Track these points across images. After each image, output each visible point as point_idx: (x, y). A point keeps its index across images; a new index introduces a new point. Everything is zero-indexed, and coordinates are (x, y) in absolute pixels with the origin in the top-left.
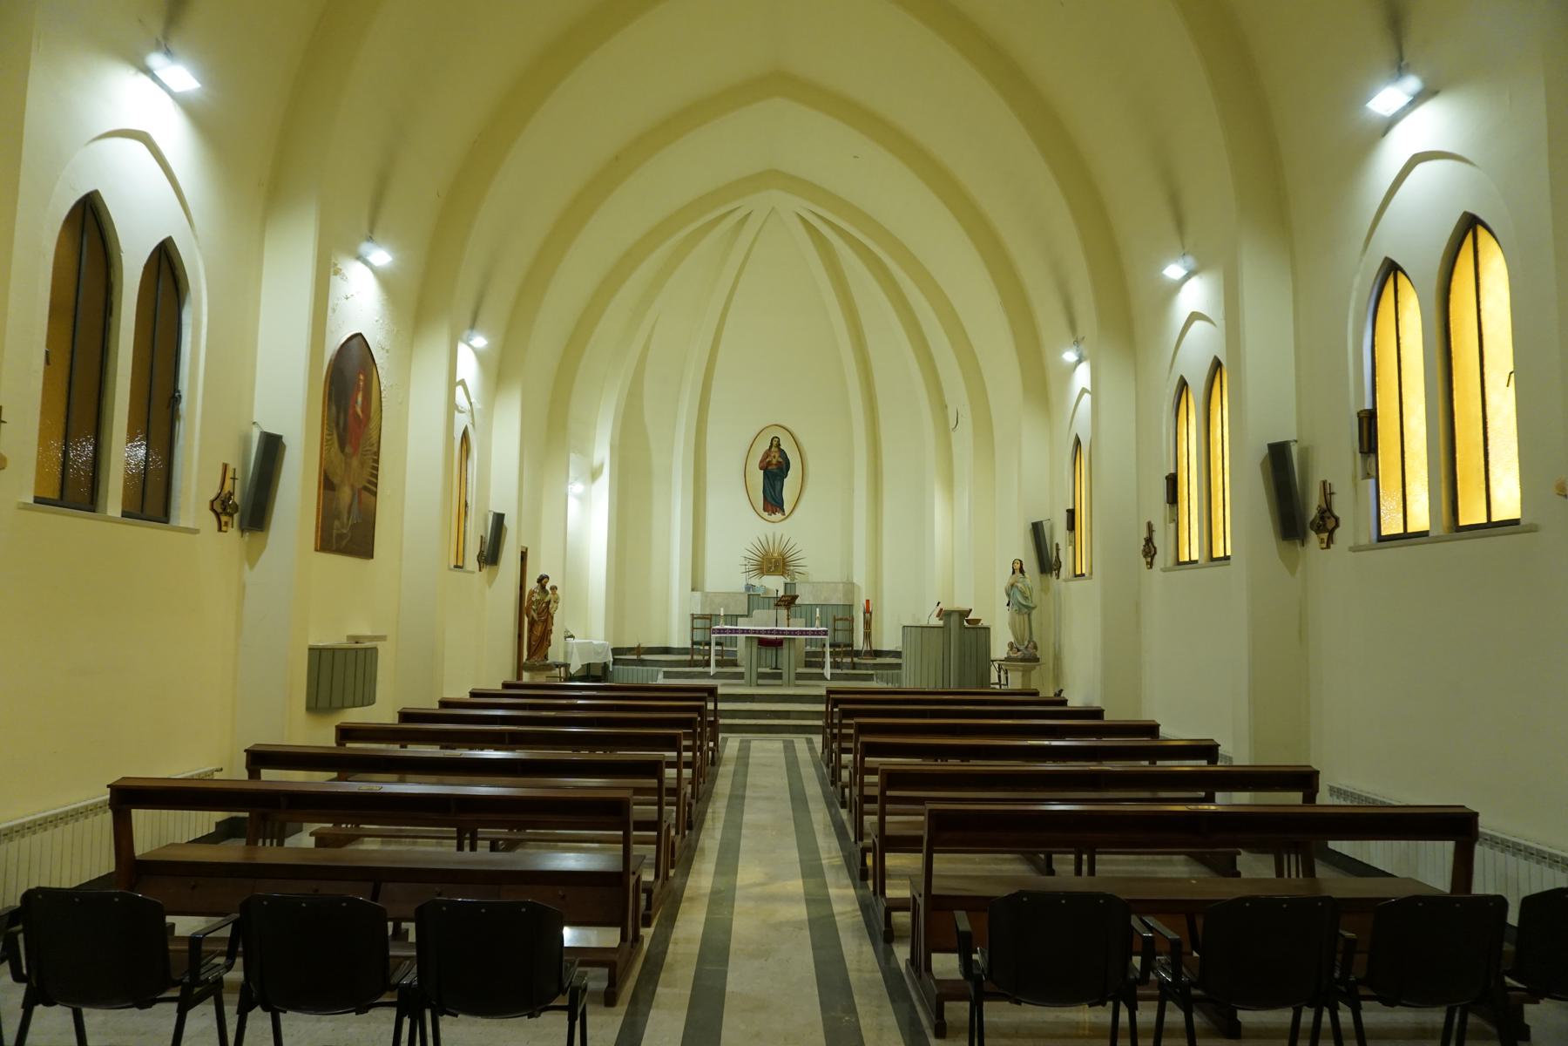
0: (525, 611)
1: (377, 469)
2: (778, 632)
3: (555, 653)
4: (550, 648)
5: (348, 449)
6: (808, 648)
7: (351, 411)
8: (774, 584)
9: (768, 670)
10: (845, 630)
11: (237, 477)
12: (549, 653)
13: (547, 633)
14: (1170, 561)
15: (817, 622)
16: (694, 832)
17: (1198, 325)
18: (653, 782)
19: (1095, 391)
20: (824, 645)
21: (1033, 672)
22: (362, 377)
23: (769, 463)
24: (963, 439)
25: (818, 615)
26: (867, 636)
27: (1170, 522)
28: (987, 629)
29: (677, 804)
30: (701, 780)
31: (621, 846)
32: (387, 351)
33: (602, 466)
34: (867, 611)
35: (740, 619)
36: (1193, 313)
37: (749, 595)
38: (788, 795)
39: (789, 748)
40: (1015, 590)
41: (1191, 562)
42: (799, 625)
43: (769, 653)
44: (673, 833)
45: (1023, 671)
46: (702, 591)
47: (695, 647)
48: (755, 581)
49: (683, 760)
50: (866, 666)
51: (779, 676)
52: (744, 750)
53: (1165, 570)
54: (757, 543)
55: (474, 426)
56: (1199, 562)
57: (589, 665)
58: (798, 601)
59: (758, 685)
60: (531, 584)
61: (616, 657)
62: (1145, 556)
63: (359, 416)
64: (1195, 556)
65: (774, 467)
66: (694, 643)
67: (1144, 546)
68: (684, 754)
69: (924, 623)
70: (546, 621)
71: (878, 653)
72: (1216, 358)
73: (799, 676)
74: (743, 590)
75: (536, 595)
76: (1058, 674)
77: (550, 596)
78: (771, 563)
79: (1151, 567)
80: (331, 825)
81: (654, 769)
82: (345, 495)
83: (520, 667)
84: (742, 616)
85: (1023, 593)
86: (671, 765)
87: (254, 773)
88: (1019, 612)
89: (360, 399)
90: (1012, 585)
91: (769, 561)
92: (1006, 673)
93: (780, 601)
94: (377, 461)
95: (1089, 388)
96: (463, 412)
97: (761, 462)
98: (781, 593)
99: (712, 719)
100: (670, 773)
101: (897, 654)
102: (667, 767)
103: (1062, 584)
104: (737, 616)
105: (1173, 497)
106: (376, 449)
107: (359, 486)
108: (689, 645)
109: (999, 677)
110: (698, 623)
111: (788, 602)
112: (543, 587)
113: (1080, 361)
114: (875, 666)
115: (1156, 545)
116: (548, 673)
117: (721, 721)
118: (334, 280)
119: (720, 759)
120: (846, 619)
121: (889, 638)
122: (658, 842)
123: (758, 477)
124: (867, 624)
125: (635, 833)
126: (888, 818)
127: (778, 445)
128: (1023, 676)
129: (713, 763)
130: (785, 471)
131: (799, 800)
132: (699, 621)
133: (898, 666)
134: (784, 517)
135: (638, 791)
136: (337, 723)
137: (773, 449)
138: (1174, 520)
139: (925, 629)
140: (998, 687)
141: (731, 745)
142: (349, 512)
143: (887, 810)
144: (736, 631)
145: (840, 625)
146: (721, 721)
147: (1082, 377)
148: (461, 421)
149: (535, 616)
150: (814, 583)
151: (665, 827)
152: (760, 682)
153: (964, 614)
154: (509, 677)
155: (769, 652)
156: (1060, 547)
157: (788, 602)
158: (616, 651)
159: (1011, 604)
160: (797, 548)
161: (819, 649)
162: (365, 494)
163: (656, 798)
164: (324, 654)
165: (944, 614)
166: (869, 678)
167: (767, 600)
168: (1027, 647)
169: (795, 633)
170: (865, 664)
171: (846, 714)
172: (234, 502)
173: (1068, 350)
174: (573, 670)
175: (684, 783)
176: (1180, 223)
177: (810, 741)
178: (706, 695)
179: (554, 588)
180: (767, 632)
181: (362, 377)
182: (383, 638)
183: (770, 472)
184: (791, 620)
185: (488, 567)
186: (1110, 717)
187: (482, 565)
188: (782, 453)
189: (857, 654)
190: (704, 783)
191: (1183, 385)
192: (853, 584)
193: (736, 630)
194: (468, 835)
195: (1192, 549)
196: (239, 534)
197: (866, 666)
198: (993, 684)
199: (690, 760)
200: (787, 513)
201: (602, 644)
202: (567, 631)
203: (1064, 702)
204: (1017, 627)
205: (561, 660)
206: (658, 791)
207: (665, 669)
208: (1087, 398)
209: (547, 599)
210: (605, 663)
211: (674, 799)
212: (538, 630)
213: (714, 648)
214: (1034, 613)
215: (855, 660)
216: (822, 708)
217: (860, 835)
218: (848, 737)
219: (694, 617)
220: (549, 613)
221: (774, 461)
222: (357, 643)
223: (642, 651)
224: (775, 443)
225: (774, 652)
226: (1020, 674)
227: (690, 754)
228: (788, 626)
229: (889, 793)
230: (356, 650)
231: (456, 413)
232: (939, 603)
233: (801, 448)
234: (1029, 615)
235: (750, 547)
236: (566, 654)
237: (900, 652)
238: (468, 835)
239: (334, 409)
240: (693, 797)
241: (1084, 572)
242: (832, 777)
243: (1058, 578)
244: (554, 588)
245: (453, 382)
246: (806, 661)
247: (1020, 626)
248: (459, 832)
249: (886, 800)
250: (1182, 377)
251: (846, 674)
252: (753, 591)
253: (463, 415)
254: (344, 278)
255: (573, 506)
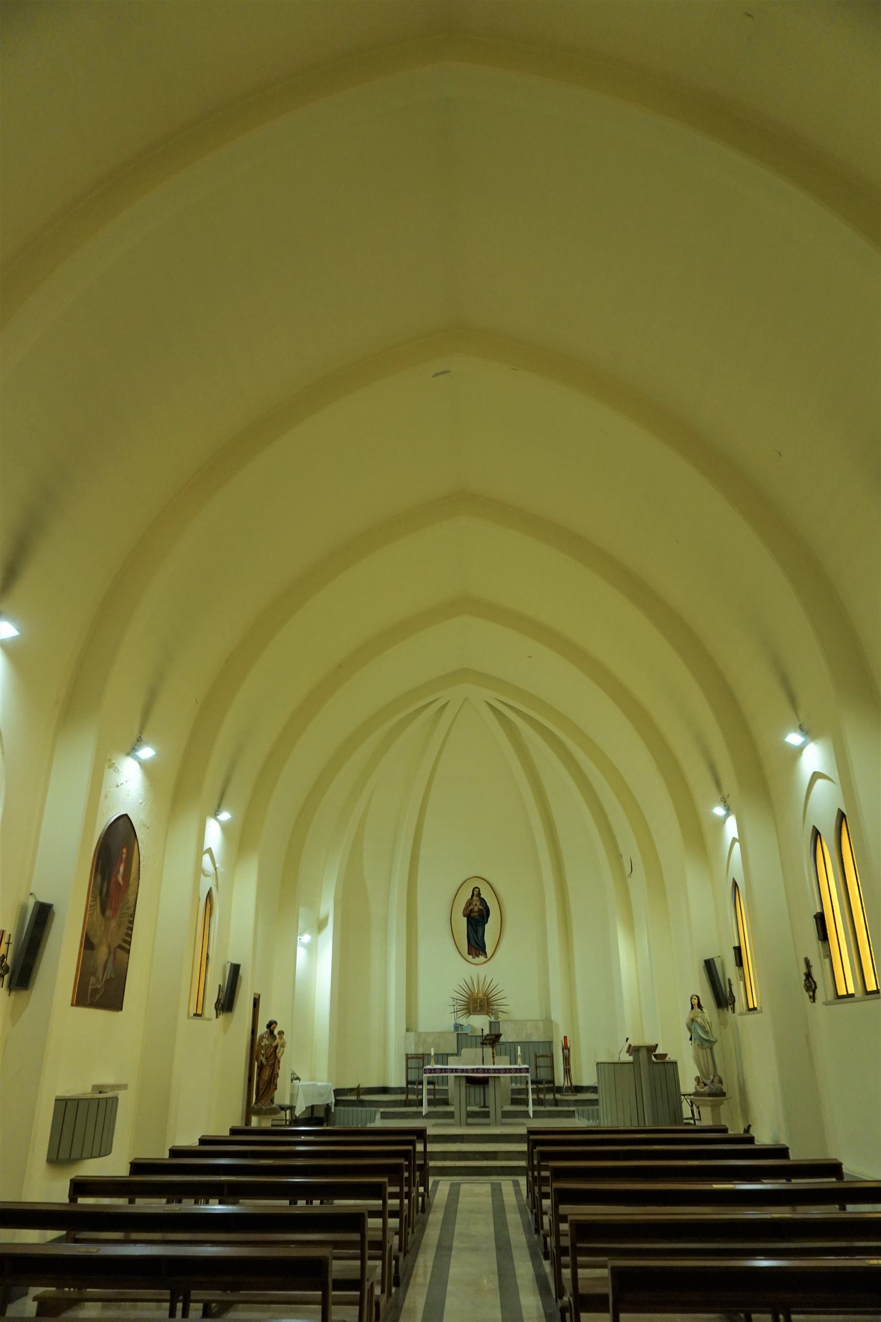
0: (255, 1056)
1: (131, 929)
2: (484, 1071)
3: (282, 1095)
4: (276, 1092)
5: (109, 913)
6: (514, 1085)
7: (113, 880)
8: (479, 1023)
9: (476, 1109)
10: (548, 1067)
11: (10, 942)
12: (275, 1096)
13: (274, 1076)
14: (831, 996)
15: (519, 1060)
16: (401, 1289)
17: (820, 783)
18: (356, 1237)
19: (742, 839)
20: (527, 1083)
21: (722, 1107)
22: (125, 851)
23: (472, 911)
24: (638, 883)
25: (519, 1053)
26: (567, 1071)
27: (824, 958)
28: (674, 1063)
29: (382, 1258)
30: (410, 1230)
31: (320, 1307)
32: (148, 828)
33: (327, 918)
34: (565, 1047)
35: (450, 1059)
36: (815, 773)
37: (457, 1034)
38: (493, 1244)
39: (497, 1191)
40: (695, 1024)
41: (850, 996)
42: (503, 1063)
43: (477, 1091)
44: (377, 1291)
45: (712, 1106)
46: (416, 1031)
47: (409, 1086)
48: (463, 1021)
49: (388, 1209)
50: (568, 1103)
51: (486, 1115)
52: (454, 1194)
53: (826, 1004)
54: (462, 983)
55: (217, 887)
56: (856, 996)
57: (312, 1106)
58: (502, 1039)
59: (468, 1124)
60: (262, 1029)
61: (339, 1098)
62: (807, 991)
63: (120, 884)
64: (851, 990)
65: (476, 914)
66: (408, 1083)
67: (805, 981)
68: (390, 1202)
69: (616, 1060)
70: (274, 1064)
71: (578, 1089)
72: (839, 810)
73: (506, 1114)
74: (452, 1029)
75: (265, 1040)
76: (745, 1109)
77: (278, 1040)
78: (476, 1002)
79: (814, 1001)
80: (54, 1289)
81: (355, 1222)
82: (102, 953)
83: (249, 1112)
84: (452, 1055)
85: (703, 1028)
86: (374, 1214)
87: (73, 1198)
88: (701, 1046)
89: (122, 869)
90: (693, 1020)
91: (475, 1001)
92: (698, 1108)
93: (485, 1039)
94: (132, 922)
95: (737, 837)
96: (208, 876)
97: (465, 910)
98: (487, 1032)
99: (422, 1162)
100: (374, 1223)
101: (594, 1089)
102: (370, 1217)
103: (737, 1017)
104: (448, 1055)
105: (823, 935)
106: (131, 912)
107: (115, 945)
108: (404, 1085)
109: (692, 1111)
110: (413, 1063)
111: (493, 1040)
112: (271, 1032)
113: (727, 815)
114: (577, 1103)
115: (815, 979)
116: (274, 1117)
117: (432, 1164)
118: (108, 772)
119: (430, 1205)
120: (546, 1056)
121: (586, 1076)
122: (361, 1303)
123: (462, 923)
124: (566, 1060)
125: (334, 1293)
126: (580, 1271)
127: (479, 894)
128: (712, 1110)
129: (423, 1210)
130: (485, 916)
131: (503, 1248)
132: (413, 1060)
133: (595, 1102)
134: (487, 959)
135: (336, 1244)
136: (72, 1177)
137: (475, 898)
138: (828, 956)
139: (616, 1066)
140: (692, 1122)
141: (441, 1188)
142: (105, 968)
143: (578, 1263)
144: (445, 1070)
145: (542, 1062)
146: (432, 1164)
147: (731, 828)
148: (206, 883)
149: (264, 1060)
150: (516, 1021)
151: (367, 1285)
152: (470, 1121)
153: (651, 1049)
154: (237, 1122)
155: (478, 1090)
156: (732, 982)
157: (493, 1040)
158: (337, 1092)
159: (693, 1039)
160: (500, 988)
161: (523, 1086)
162: (120, 952)
163: (359, 1251)
164: (69, 1103)
165: (633, 1050)
166: (570, 1115)
167: (475, 1038)
168: (712, 1082)
169: (498, 1071)
170: (566, 1101)
171: (544, 1156)
172: (6, 964)
173: (716, 806)
174: (298, 1113)
175: (389, 1234)
176: (793, 701)
177: (516, 1184)
178: (414, 1138)
179: (281, 1033)
180: (473, 1071)
181: (125, 851)
182: (124, 1087)
183: (473, 918)
184: (496, 1058)
185: (224, 1014)
186: (796, 1156)
187: (219, 1012)
188: (483, 901)
189: (559, 1090)
190: (413, 1232)
191: (816, 834)
192: (551, 1021)
193: (445, 1069)
194: (181, 1298)
195: (848, 984)
196: (7, 993)
197: (568, 1103)
198: (685, 1119)
199: (398, 1208)
200: (489, 955)
201: (326, 1085)
202: (293, 1074)
203: (751, 1140)
204: (701, 1059)
205: (287, 1102)
206: (361, 1244)
207: (382, 1110)
208: (737, 845)
209: (274, 1044)
210: (328, 1104)
211: (379, 1253)
212: (267, 1073)
213: (425, 1087)
214: (716, 1047)
215: (558, 1096)
216: (524, 1147)
217: (560, 1293)
218: (545, 1180)
219: (408, 1057)
220: (276, 1057)
221: (476, 909)
222: (100, 1092)
223: (356, 1092)
224: (476, 893)
225: (482, 1090)
226: (709, 1108)
227: (397, 1201)
228: (494, 1064)
229: (579, 1245)
230: (99, 1099)
231: (202, 876)
232: (627, 1039)
233: (499, 897)
234: (711, 1049)
235: (457, 988)
236: (293, 1096)
237: (596, 1087)
238: (181, 1298)
239: (99, 878)
240: (400, 1249)
241: (756, 1006)
242: (536, 1225)
243: (734, 1012)
244: (281, 1033)
245: (201, 850)
246: (512, 1099)
247: (704, 1058)
248: (172, 1294)
249: (577, 1252)
250: (814, 827)
251: (550, 1111)
252: (461, 1031)
253: (209, 878)
254: (117, 771)
255: (301, 954)
